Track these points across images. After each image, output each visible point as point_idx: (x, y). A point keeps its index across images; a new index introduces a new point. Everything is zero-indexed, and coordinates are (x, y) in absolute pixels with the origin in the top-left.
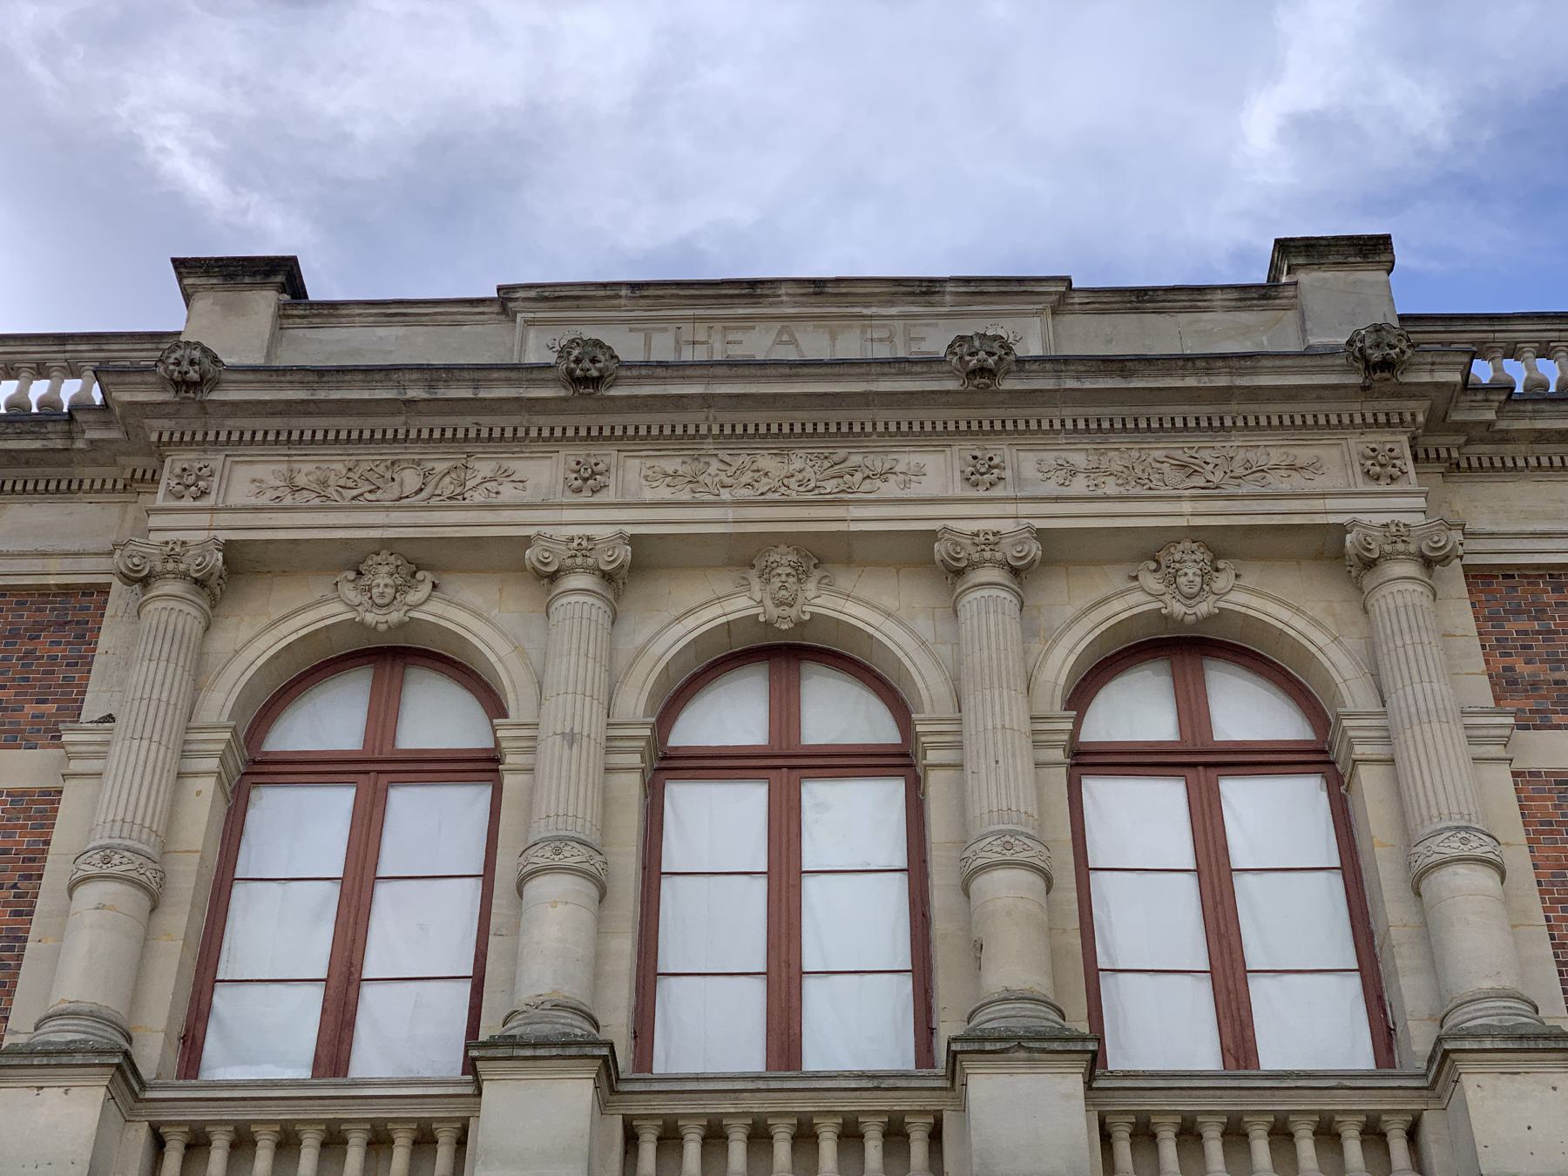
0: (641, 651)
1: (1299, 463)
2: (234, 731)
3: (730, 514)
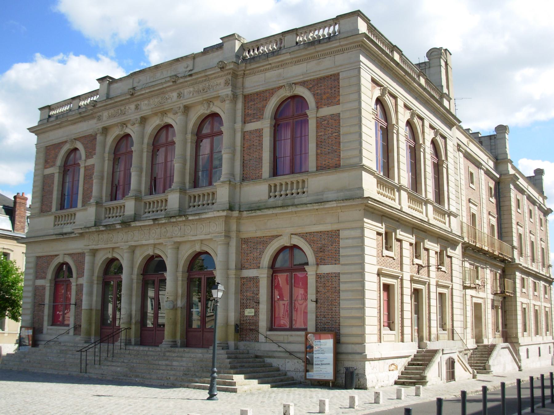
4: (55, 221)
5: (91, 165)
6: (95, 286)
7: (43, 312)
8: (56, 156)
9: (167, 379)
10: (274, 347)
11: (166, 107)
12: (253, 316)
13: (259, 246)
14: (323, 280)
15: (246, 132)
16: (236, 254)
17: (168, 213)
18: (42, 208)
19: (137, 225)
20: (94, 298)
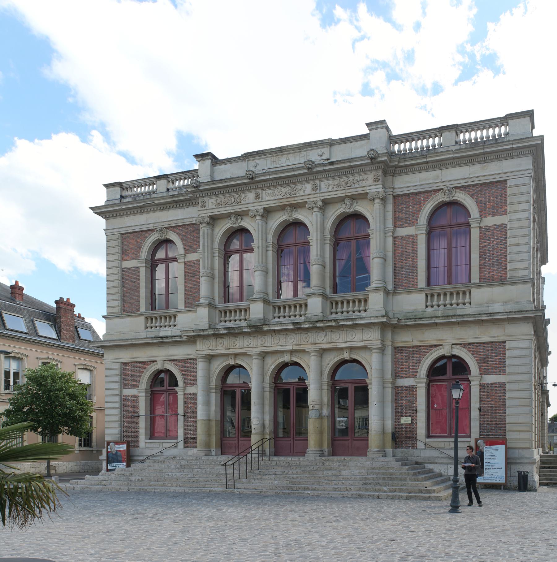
0: (271, 228)
1: (365, 179)
2: (330, 235)
3: (344, 191)
4: (146, 323)
5: (194, 261)
6: (213, 396)
7: (137, 424)
8: (139, 247)
9: (347, 490)
10: (435, 454)
11: (298, 200)
12: (409, 424)
13: (415, 356)
14: (486, 390)
15: (396, 237)
16: (392, 362)
17: (309, 317)
18: (123, 307)
19: (272, 328)
20: (213, 408)
